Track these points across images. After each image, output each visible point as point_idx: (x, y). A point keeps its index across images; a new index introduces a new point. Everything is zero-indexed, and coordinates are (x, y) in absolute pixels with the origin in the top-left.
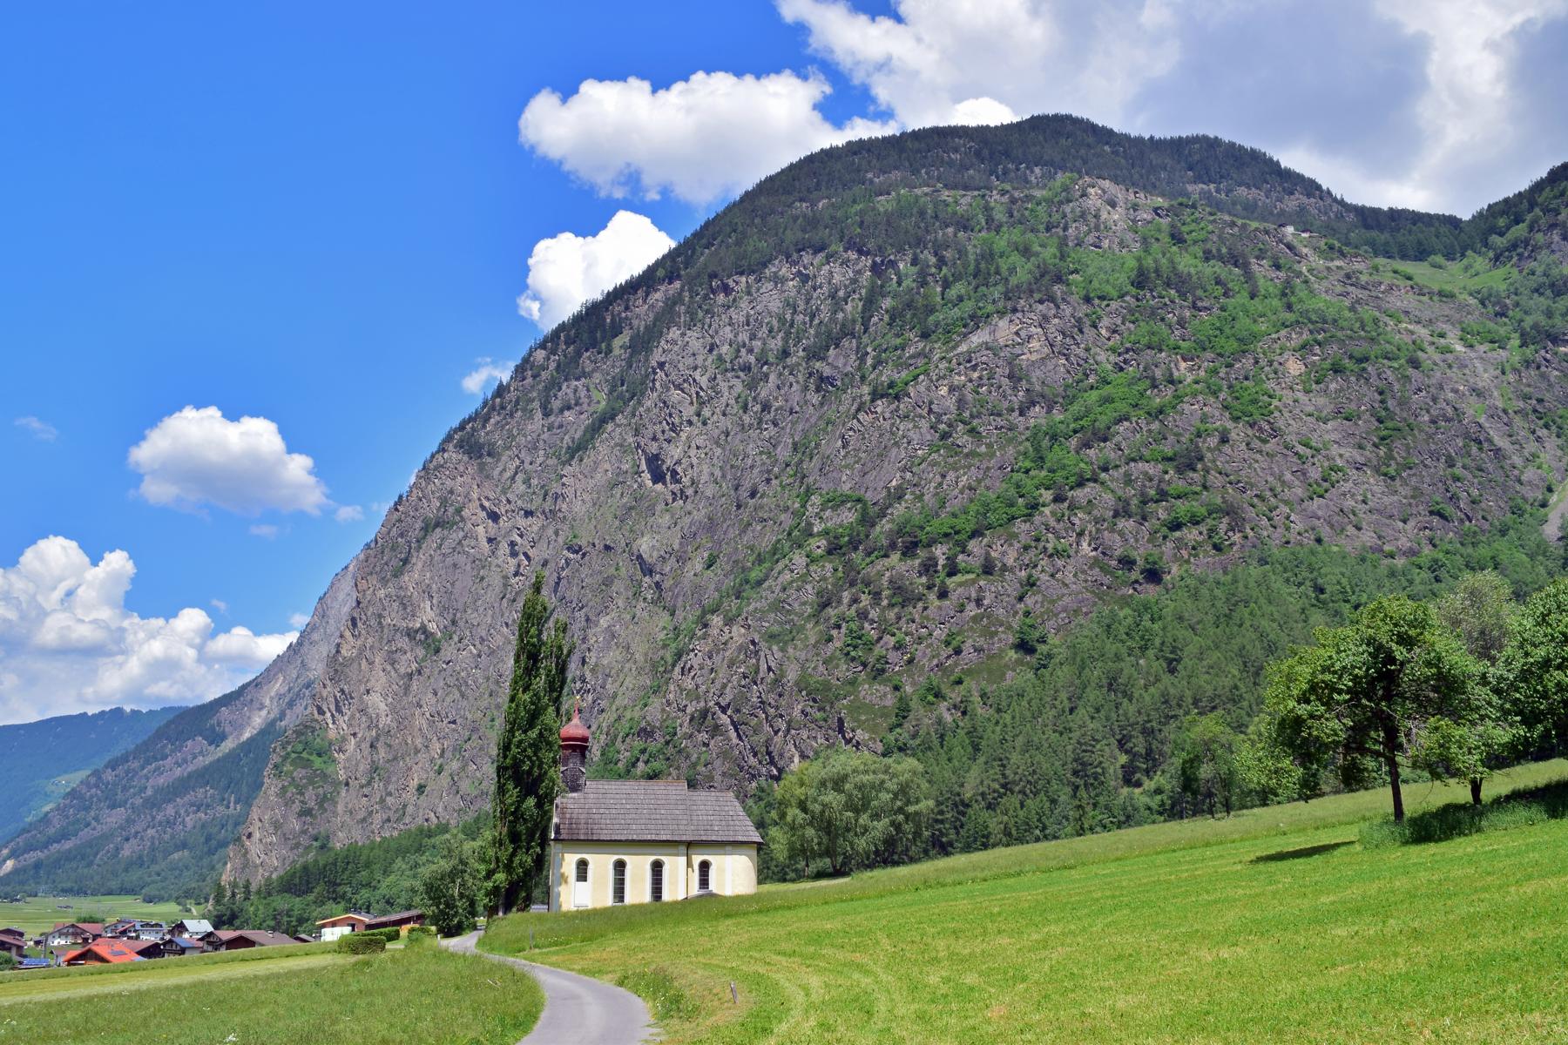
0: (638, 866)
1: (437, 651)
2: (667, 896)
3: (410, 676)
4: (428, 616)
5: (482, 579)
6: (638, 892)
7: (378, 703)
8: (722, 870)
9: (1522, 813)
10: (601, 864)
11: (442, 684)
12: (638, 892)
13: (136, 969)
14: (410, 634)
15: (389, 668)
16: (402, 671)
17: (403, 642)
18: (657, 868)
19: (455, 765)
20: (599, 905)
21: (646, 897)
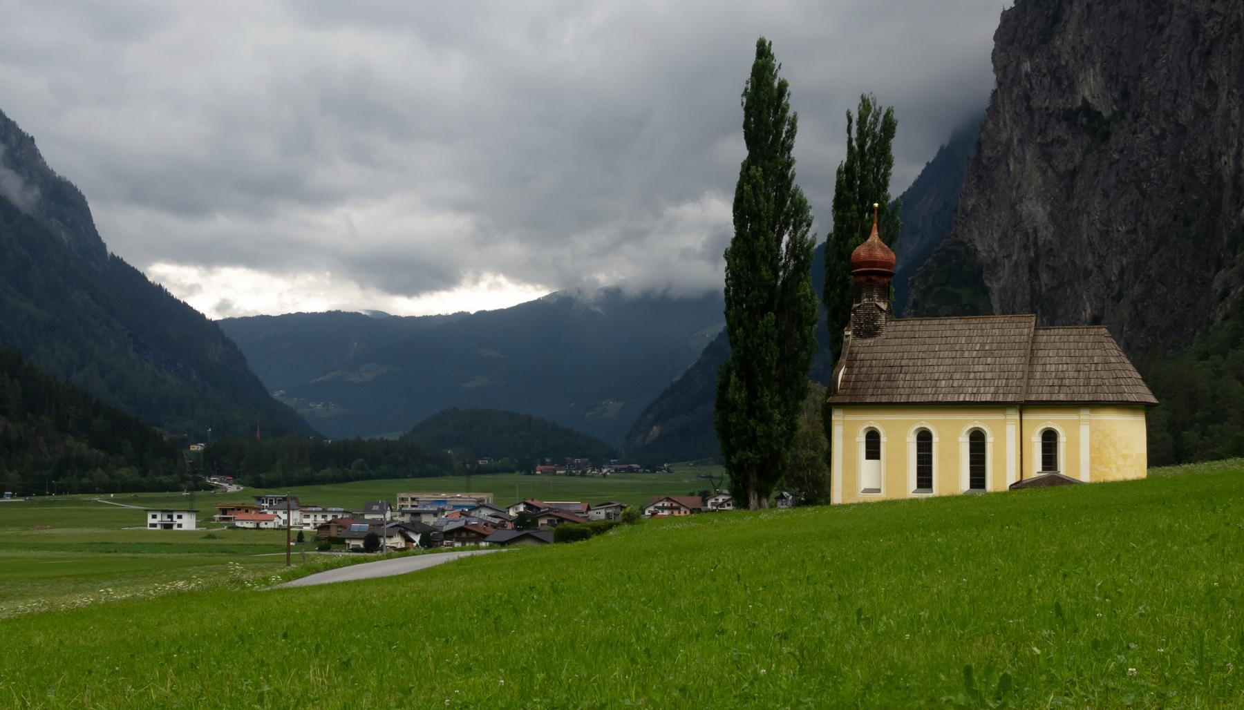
0: (951, 435)
1: (1106, 137)
2: (990, 486)
3: (1073, 173)
4: (1091, 87)
5: (1162, 28)
6: (952, 476)
7: (1036, 211)
8: (1074, 444)
9: (324, 416)
10: (899, 432)
11: (1113, 180)
12: (952, 476)
13: (356, 561)
14: (1069, 117)
15: (1044, 165)
16: (1062, 168)
17: (1059, 130)
18: (977, 441)
19: (1138, 289)
20: (896, 495)
21: (964, 484)
